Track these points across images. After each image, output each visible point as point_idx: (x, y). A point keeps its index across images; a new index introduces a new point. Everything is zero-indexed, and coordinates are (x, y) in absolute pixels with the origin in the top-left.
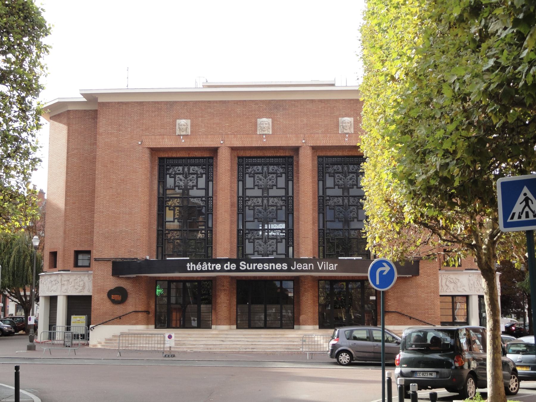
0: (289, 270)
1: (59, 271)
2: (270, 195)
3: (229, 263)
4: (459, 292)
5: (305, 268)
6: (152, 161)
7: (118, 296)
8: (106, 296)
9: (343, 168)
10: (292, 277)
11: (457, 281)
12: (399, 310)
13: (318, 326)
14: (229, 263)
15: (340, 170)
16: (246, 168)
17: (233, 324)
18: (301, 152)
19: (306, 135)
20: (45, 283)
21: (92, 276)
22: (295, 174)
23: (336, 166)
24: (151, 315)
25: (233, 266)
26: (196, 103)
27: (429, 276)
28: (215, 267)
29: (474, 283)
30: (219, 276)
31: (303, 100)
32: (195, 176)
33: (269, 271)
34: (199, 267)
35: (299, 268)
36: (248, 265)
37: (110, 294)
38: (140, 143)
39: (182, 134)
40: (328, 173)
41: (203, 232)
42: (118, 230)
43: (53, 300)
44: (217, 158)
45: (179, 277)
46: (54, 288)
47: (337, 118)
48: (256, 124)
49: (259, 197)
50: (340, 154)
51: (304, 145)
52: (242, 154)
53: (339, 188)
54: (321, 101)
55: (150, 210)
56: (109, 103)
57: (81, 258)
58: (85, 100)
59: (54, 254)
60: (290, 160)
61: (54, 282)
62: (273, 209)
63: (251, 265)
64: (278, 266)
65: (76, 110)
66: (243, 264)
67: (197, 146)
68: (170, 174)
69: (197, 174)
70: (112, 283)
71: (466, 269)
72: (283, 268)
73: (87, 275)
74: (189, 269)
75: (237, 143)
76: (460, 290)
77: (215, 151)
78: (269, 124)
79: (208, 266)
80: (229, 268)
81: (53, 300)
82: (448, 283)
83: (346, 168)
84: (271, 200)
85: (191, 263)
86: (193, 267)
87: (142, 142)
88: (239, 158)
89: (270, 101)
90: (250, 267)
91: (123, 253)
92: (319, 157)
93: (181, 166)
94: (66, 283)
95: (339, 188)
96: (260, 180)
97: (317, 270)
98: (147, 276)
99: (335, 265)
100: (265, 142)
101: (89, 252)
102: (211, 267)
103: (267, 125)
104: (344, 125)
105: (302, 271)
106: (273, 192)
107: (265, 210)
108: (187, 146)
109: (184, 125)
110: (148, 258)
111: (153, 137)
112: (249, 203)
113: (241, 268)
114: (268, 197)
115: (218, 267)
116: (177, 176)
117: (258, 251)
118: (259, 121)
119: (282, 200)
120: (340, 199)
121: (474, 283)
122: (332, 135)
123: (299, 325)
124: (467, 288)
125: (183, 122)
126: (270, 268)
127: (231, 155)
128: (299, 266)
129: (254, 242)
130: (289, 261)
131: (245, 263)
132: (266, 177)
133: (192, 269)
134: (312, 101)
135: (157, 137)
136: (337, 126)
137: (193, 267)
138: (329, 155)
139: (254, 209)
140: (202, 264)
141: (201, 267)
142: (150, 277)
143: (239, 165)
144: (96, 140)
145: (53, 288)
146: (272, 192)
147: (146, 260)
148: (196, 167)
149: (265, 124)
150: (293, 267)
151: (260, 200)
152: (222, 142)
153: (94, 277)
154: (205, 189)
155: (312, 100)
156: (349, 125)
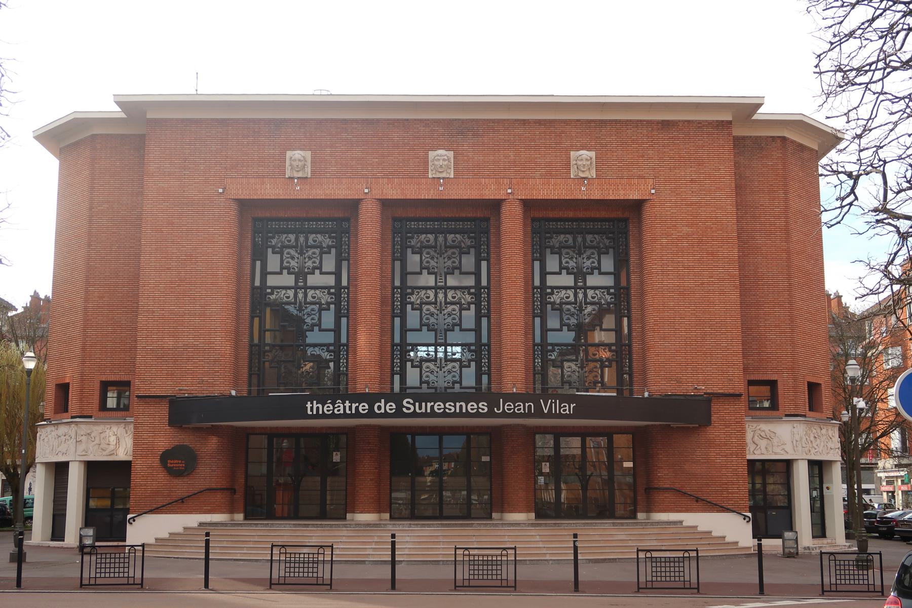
0: (491, 414)
1: (72, 417)
2: (588, 284)
3: (383, 401)
4: (776, 454)
5: (565, 410)
6: (241, 224)
7: (178, 462)
8: (156, 462)
9: (574, 240)
10: (488, 427)
11: (772, 435)
12: (677, 486)
13: (533, 515)
14: (383, 401)
15: (571, 242)
16: (546, 238)
17: (385, 512)
18: (505, 209)
19: (514, 181)
20: (46, 440)
21: (132, 426)
22: (492, 249)
23: (562, 236)
24: (239, 496)
25: (391, 407)
26: (320, 122)
27: (727, 426)
28: (357, 408)
29: (801, 438)
30: (361, 426)
31: (508, 120)
32: (317, 251)
33: (454, 415)
34: (327, 408)
35: (509, 409)
36: (417, 404)
37: (165, 457)
38: (221, 190)
39: (296, 175)
40: (270, 247)
41: (332, 348)
42: (180, 344)
43: (60, 470)
44: (357, 220)
45: (289, 428)
46: (63, 448)
47: (567, 151)
48: (426, 162)
49: (290, 288)
50: (603, 214)
51: (511, 197)
52: (260, 214)
53: (289, 273)
54: (539, 122)
55: (238, 309)
56: (166, 120)
57: (114, 395)
58: (124, 116)
59: (63, 389)
60: (345, 225)
61: (63, 438)
62: (313, 310)
63: (423, 404)
64: (472, 407)
65: (108, 135)
66: (408, 402)
67: (323, 197)
68: (273, 247)
69: (321, 247)
70: (165, 439)
71: (787, 416)
72: (447, 411)
73: (123, 425)
74: (309, 413)
75: (393, 193)
76: (778, 450)
77: (496, 205)
78: (449, 160)
79: (345, 407)
80: (383, 411)
81: (60, 470)
82: (756, 437)
83: (580, 239)
84: (311, 293)
85: (315, 402)
86: (318, 408)
87: (224, 189)
88: (395, 219)
89: (450, 122)
90: (420, 408)
91: (188, 386)
92: (395, 219)
93: (292, 233)
94: (84, 438)
95: (289, 273)
96: (432, 258)
97: (539, 413)
98: (232, 426)
99: (572, 406)
100: (583, 193)
101: (127, 384)
102: (350, 408)
103: (446, 163)
104: (579, 163)
105: (514, 415)
106: (314, 279)
107: (581, 310)
108: (305, 197)
109: (300, 160)
110: (233, 393)
111: (244, 181)
112: (413, 298)
113: (404, 409)
114: (446, 288)
115: (363, 407)
116: (286, 251)
117: (427, 325)
118: (432, 154)
119: (470, 294)
120: (571, 293)
121: (801, 438)
122: (559, 181)
123: (502, 512)
124: (789, 448)
125: (297, 154)
126: (458, 411)
127: (382, 213)
128: (508, 407)
129: (420, 367)
130: (493, 398)
131: (412, 401)
132: (301, 254)
133: (315, 413)
134: (524, 122)
135: (253, 181)
136: (568, 165)
137: (318, 408)
138: (551, 216)
139: (560, 310)
140: (333, 404)
141: (331, 408)
142: (237, 428)
143: (395, 232)
144: (142, 188)
145: (60, 449)
146: (312, 280)
147: (231, 396)
148: (319, 236)
149: (583, 159)
150: (499, 409)
151: (571, 293)
152: (366, 191)
153: (135, 428)
154: (475, 274)
155: (524, 120)
156: (589, 163)
